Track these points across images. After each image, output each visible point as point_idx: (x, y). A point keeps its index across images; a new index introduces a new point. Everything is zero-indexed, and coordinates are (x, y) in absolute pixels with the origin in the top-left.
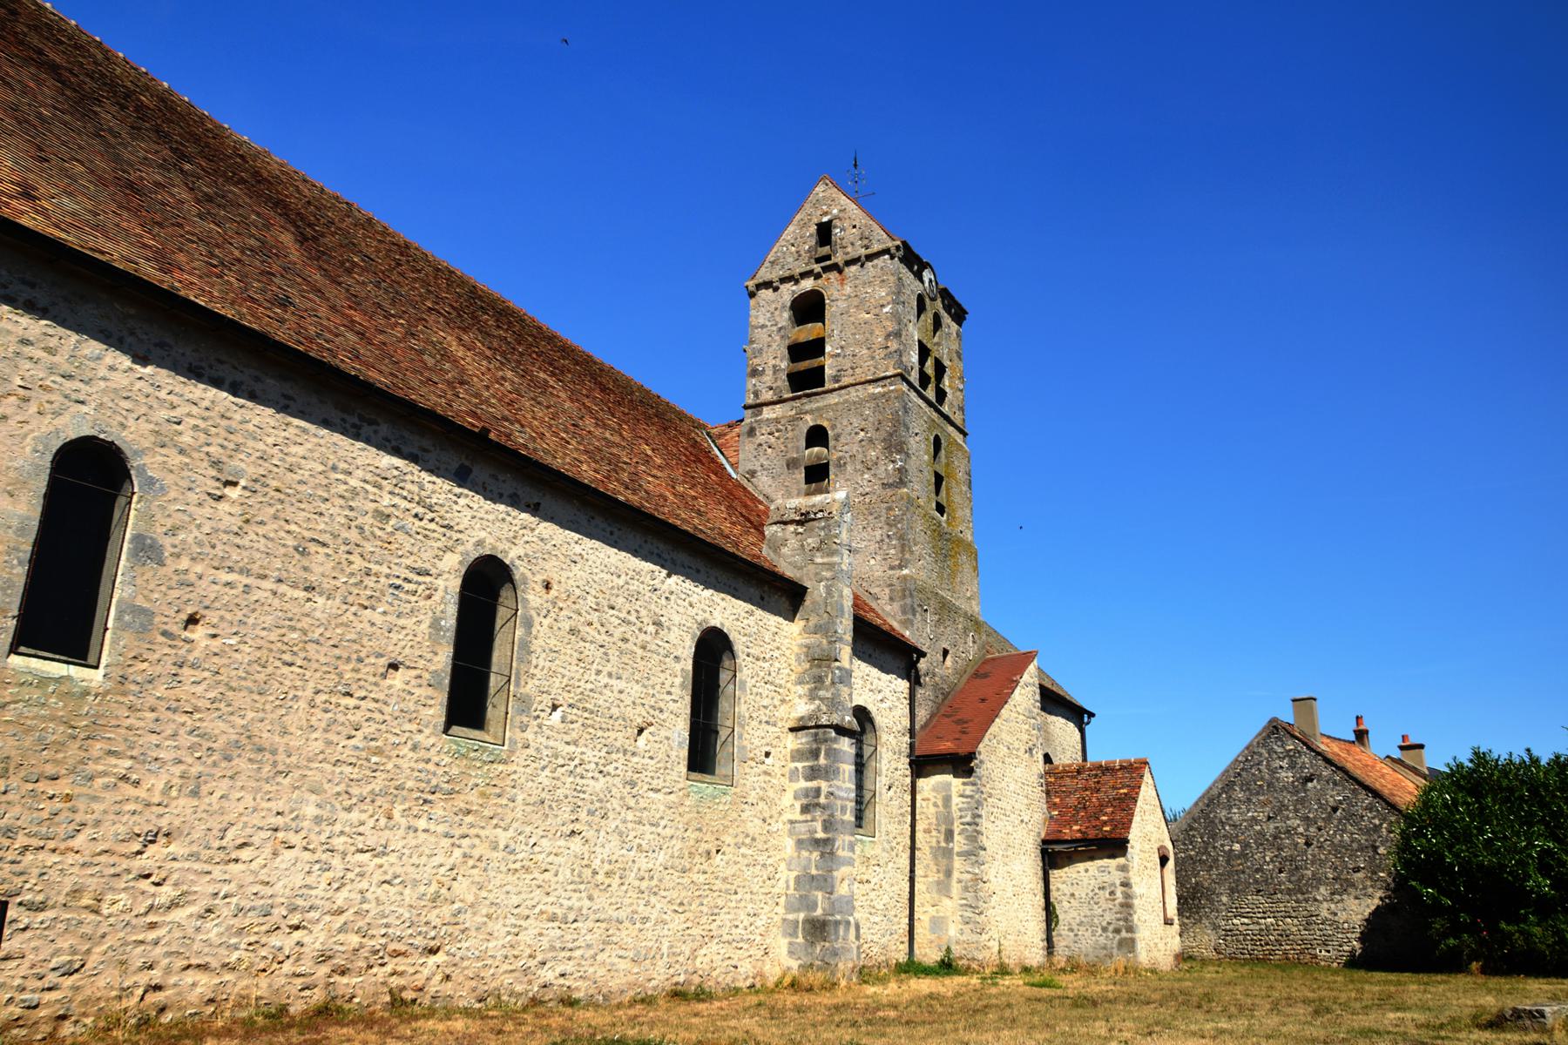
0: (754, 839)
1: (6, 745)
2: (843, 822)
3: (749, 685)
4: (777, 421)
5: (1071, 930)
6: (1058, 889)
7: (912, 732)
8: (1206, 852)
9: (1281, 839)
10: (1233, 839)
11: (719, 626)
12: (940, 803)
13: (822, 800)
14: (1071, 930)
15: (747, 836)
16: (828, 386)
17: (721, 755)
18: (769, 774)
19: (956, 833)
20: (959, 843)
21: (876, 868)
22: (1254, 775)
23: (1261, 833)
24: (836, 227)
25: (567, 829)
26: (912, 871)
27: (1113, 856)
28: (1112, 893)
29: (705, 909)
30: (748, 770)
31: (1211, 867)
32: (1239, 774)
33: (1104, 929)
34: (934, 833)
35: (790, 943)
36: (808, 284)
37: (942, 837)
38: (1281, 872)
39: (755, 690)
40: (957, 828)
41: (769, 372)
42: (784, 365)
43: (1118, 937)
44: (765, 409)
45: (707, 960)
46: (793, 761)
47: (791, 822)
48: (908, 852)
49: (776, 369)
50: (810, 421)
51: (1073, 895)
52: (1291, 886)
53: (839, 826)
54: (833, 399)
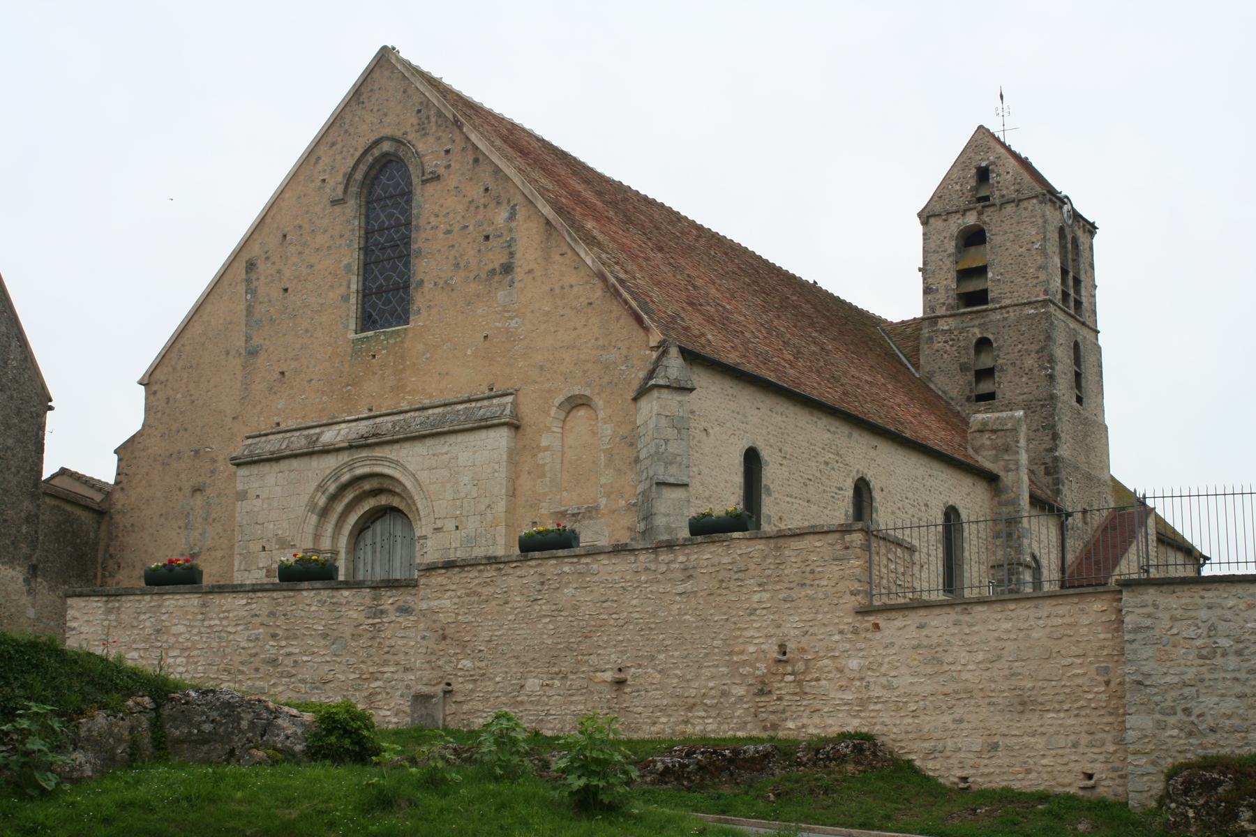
1: (3, 601)
7: (1063, 569)
24: (993, 171)
36: (971, 219)
41: (942, 290)
42: (954, 286)
49: (947, 289)
50: (977, 333)
54: (997, 316)
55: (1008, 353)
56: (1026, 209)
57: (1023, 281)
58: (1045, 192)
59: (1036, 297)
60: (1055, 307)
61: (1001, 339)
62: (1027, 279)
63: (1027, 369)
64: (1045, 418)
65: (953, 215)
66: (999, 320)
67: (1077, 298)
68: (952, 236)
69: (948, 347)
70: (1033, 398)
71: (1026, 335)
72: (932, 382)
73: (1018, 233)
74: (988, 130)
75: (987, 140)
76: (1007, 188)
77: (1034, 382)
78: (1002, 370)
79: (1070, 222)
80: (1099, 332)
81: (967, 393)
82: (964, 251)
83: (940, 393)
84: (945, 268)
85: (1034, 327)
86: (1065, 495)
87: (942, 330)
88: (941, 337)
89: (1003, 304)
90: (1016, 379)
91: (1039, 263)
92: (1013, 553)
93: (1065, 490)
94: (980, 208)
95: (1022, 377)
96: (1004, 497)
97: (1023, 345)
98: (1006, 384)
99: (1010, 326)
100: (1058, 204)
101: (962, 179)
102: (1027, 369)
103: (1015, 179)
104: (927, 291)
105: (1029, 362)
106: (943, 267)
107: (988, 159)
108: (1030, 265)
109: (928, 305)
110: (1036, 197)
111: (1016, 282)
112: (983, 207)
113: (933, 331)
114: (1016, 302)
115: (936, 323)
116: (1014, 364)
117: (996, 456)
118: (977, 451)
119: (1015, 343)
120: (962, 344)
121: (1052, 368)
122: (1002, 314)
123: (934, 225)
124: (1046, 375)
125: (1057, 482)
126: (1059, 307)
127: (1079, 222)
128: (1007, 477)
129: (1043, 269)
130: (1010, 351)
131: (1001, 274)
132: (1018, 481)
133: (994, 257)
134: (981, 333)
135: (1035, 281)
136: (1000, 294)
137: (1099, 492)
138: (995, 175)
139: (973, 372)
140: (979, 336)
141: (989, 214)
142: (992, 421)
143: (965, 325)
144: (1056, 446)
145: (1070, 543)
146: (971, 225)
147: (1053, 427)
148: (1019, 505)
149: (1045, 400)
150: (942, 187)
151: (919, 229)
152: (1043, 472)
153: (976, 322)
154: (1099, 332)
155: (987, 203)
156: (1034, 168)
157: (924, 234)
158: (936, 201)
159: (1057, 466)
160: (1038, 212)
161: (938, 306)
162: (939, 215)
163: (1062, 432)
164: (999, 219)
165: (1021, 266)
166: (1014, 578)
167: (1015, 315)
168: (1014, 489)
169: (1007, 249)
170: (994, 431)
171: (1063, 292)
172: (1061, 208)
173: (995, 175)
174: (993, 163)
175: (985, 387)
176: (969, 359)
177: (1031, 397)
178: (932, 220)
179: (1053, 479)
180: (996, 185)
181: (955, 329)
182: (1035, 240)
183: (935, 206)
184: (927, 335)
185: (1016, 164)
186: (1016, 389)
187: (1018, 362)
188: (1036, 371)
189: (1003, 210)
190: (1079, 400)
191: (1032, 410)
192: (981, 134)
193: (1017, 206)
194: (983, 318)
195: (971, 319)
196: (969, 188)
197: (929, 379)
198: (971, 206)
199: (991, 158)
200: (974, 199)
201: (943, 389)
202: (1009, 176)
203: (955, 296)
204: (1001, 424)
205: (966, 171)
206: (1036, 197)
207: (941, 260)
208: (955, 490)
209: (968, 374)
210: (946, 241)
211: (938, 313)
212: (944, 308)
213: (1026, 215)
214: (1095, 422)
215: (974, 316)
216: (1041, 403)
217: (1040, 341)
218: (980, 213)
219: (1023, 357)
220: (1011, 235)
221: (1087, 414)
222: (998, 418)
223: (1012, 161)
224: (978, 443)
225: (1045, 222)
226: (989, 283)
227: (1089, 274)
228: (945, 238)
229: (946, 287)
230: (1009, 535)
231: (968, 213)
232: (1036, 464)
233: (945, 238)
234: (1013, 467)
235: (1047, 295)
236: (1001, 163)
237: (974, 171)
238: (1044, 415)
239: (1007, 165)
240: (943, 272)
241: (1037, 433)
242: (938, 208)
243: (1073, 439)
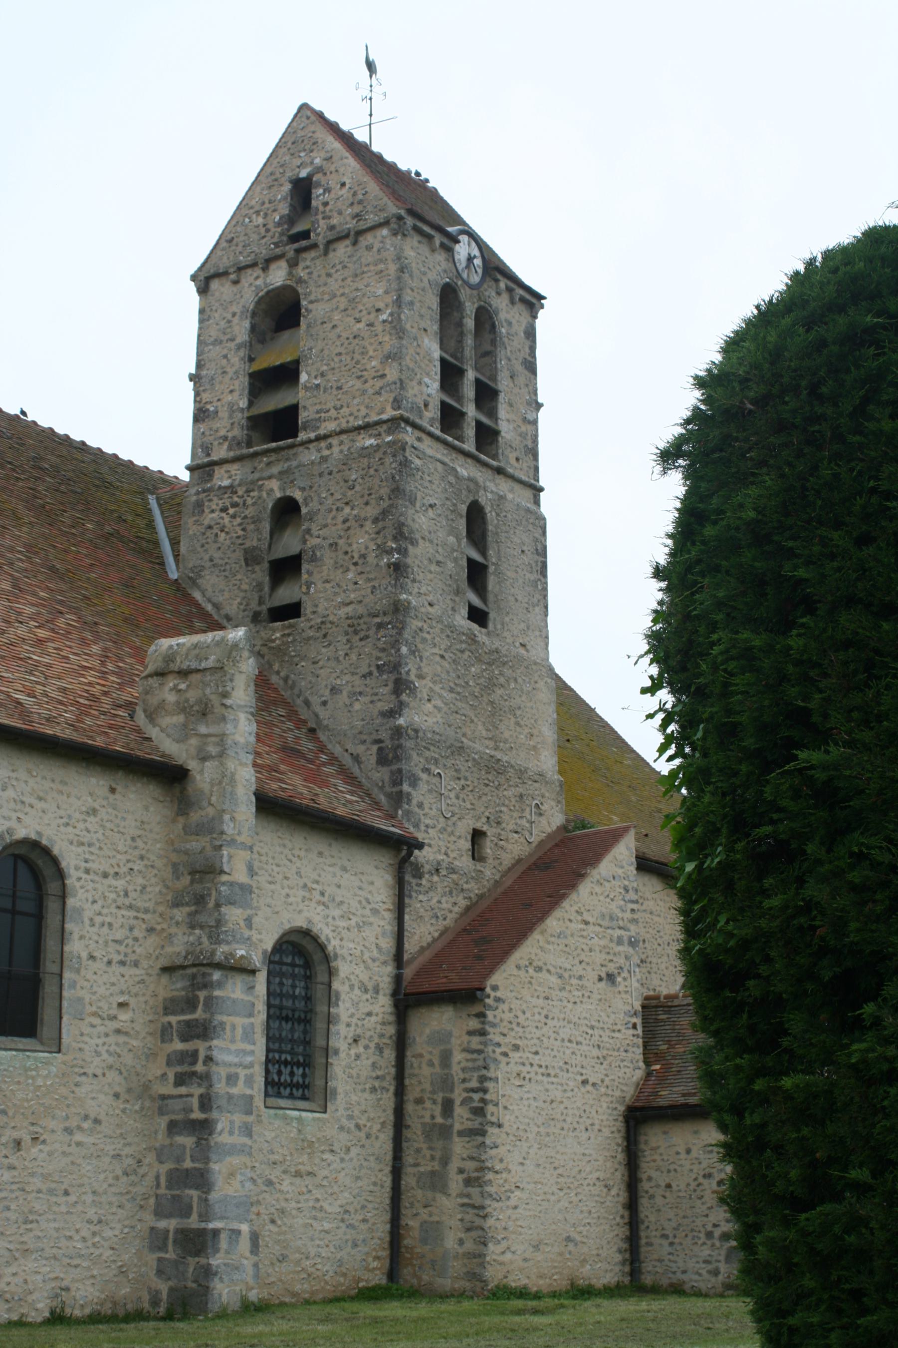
0: (97, 1121)
2: (230, 1097)
3: (87, 914)
4: (232, 489)
6: (650, 1179)
11: (33, 836)
12: (436, 1062)
13: (199, 1067)
15: (86, 1117)
17: (47, 1013)
18: (126, 1034)
19: (457, 1102)
20: (461, 1117)
21: (327, 1156)
24: (319, 185)
25: (534, 1050)
29: (13, 1216)
30: (87, 1030)
33: (709, 1235)
34: (428, 1104)
35: (160, 1260)
36: (278, 276)
37: (438, 1110)
39: (98, 920)
40: (458, 1096)
41: (224, 414)
42: (243, 403)
45: (18, 1280)
46: (166, 1014)
47: (163, 1097)
48: (389, 1132)
50: (275, 489)
51: (669, 1186)
53: (223, 1102)
54: (309, 456)
55: (326, 526)
56: (369, 248)
57: (358, 384)
58: (402, 212)
59: (379, 414)
60: (418, 433)
61: (316, 499)
62: (366, 382)
63: (356, 556)
64: (383, 650)
65: (249, 271)
66: (313, 463)
67: (485, 420)
68: (245, 309)
69: (227, 520)
70: (365, 612)
71: (358, 488)
72: (198, 587)
73: (355, 294)
74: (320, 116)
75: (312, 128)
76: (340, 213)
77: (369, 580)
78: (314, 559)
79: (475, 279)
80: (541, 490)
81: (254, 606)
82: (272, 339)
83: (209, 608)
84: (231, 371)
85: (372, 472)
86: (420, 805)
87: (220, 487)
88: (215, 500)
89: (322, 432)
90: (338, 575)
91: (387, 348)
92: (205, 940)
93: (420, 794)
94: (291, 254)
95: (348, 570)
96: (195, 817)
97: (352, 509)
98: (320, 586)
99: (330, 473)
100: (438, 239)
101: (267, 205)
102: (356, 556)
103: (355, 194)
104: (200, 415)
105: (362, 540)
106: (228, 370)
107: (312, 163)
108: (371, 353)
109: (199, 442)
110: (386, 223)
111: (345, 388)
112: (298, 251)
113: (204, 491)
114: (344, 425)
115: (211, 475)
116: (334, 546)
117: (185, 726)
118: (151, 717)
119: (339, 504)
120: (250, 512)
121: (403, 552)
122: (319, 451)
123: (217, 294)
124: (389, 565)
125: (397, 778)
126: (430, 435)
127: (497, 281)
128: (201, 772)
129: (393, 360)
130: (329, 521)
131: (323, 375)
132: (226, 781)
133: (311, 343)
134: (282, 489)
135: (379, 384)
136: (318, 412)
137: (521, 796)
138: (321, 191)
139: (266, 565)
140: (278, 495)
141: (308, 263)
142: (185, 649)
143: (257, 475)
144: (401, 705)
145: (417, 904)
146: (277, 288)
147: (396, 667)
148: (222, 833)
149: (385, 614)
150: (234, 223)
151: (193, 300)
152: (373, 759)
153: (275, 470)
154: (541, 490)
155: (304, 243)
156: (441, 199)
157: (202, 311)
158: (224, 249)
159: (400, 746)
160: (390, 253)
161: (216, 443)
162: (225, 274)
163: (420, 677)
164: (323, 273)
165: (357, 356)
166: (202, 995)
167: (341, 451)
168: (214, 799)
169: (334, 327)
170: (184, 674)
171: (445, 408)
172: (449, 250)
173: (321, 191)
174: (320, 170)
175: (286, 594)
176: (259, 540)
177: (361, 610)
178: (215, 285)
179: (392, 773)
180: (321, 208)
181: (239, 485)
182: (381, 305)
183: (221, 258)
184: (194, 498)
185: (358, 166)
186: (336, 594)
187: (341, 542)
188: (371, 559)
189: (331, 255)
190: (478, 616)
191: (362, 634)
192: (304, 119)
193: (355, 243)
194: (287, 460)
195: (269, 464)
196: (277, 218)
197: (194, 582)
198: (278, 251)
199: (317, 161)
200: (285, 238)
201: (215, 600)
202: (344, 191)
203: (244, 422)
204: (197, 656)
205: (275, 189)
206: (386, 223)
207: (225, 357)
208: (40, 805)
209: (257, 568)
210: (236, 320)
211: (214, 457)
212: (225, 446)
213: (370, 259)
214: (520, 659)
215: (273, 457)
216: (378, 620)
217: (381, 498)
218: (293, 264)
219: (351, 532)
220: (343, 299)
221: (497, 644)
222: (195, 646)
223: (351, 162)
224: (154, 701)
225: (402, 270)
226: (302, 393)
227: (521, 380)
228: (234, 315)
229: (231, 405)
230: (200, 900)
231: (273, 266)
232: (364, 742)
233: (234, 315)
234: (213, 750)
235: (399, 408)
236: (333, 169)
237: (287, 187)
238: (380, 644)
239: (342, 170)
240: (227, 378)
241: (368, 681)
242: (225, 263)
243: (451, 690)
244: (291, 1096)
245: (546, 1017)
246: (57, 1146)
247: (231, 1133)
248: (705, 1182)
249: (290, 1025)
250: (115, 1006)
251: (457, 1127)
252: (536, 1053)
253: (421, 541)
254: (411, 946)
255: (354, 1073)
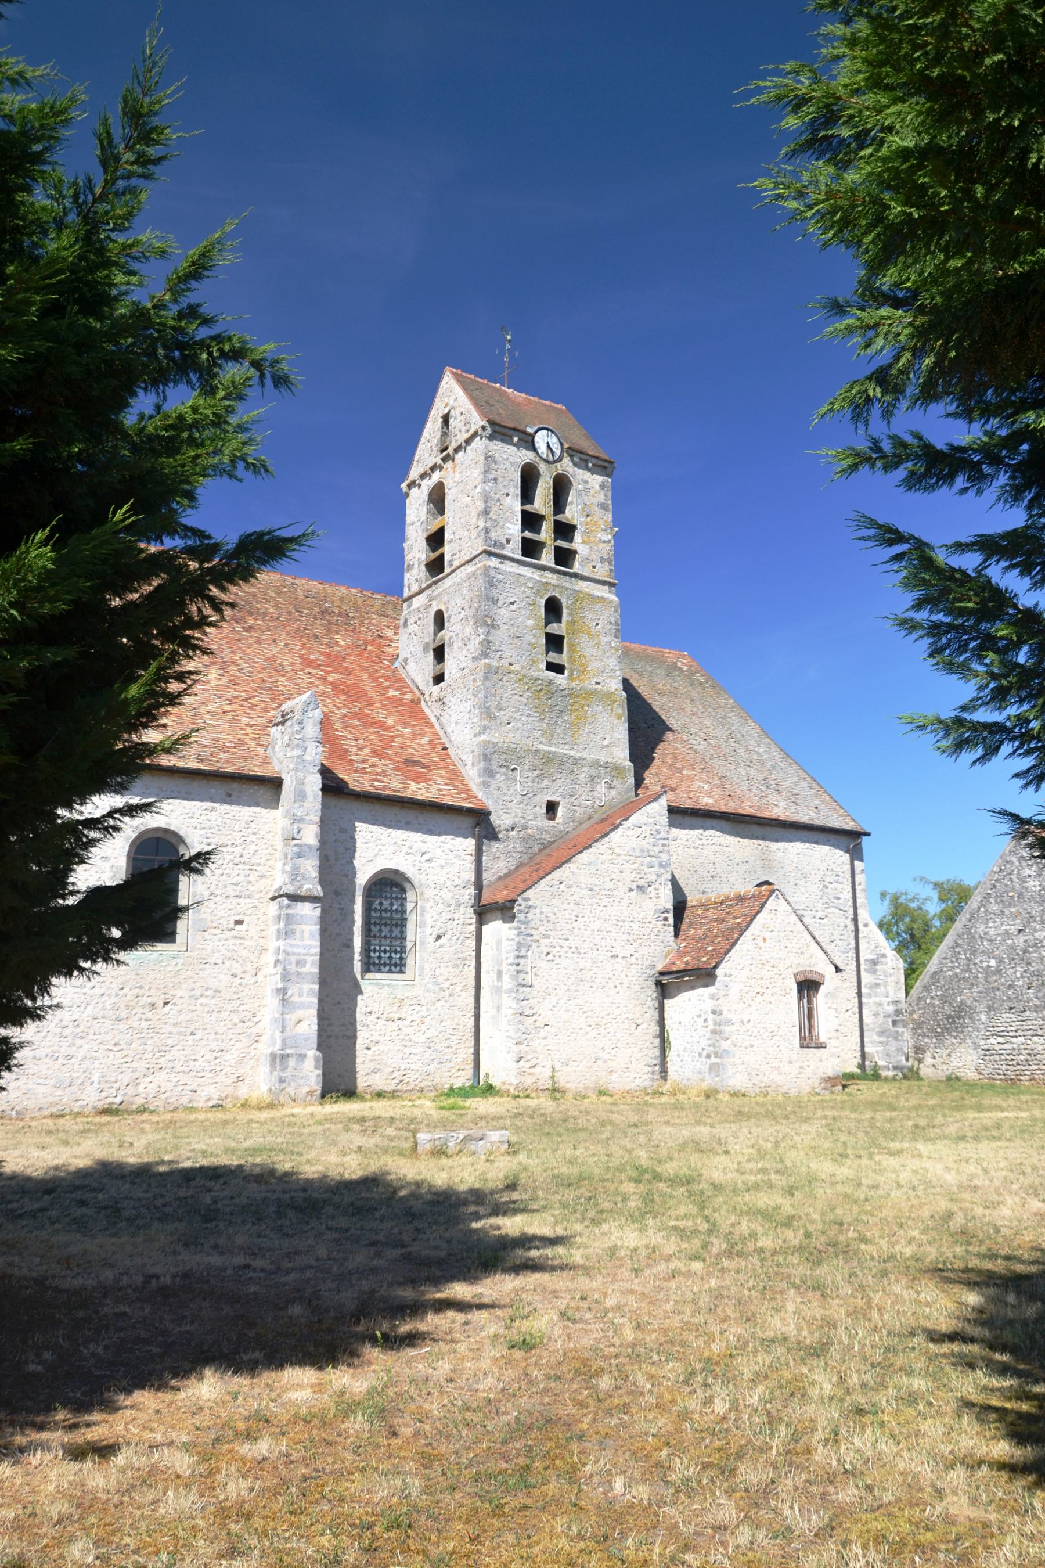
2: (299, 974)
5: (679, 1055)
8: (969, 970)
9: (1030, 953)
10: (989, 954)
14: (679, 1055)
16: (447, 570)
22: (1006, 885)
23: (1013, 947)
26: (477, 1007)
27: (706, 986)
28: (705, 1020)
31: (972, 984)
32: (994, 886)
33: (700, 1055)
38: (1029, 988)
43: (709, 1062)
44: (414, 600)
52: (1038, 1003)
244: (390, 971)
245: (577, 916)
246: (184, 1006)
247: (300, 996)
248: (698, 1020)
249: (389, 928)
250: (232, 922)
251: (504, 988)
252: (567, 940)
253: (502, 626)
254: (488, 877)
255: (437, 955)
